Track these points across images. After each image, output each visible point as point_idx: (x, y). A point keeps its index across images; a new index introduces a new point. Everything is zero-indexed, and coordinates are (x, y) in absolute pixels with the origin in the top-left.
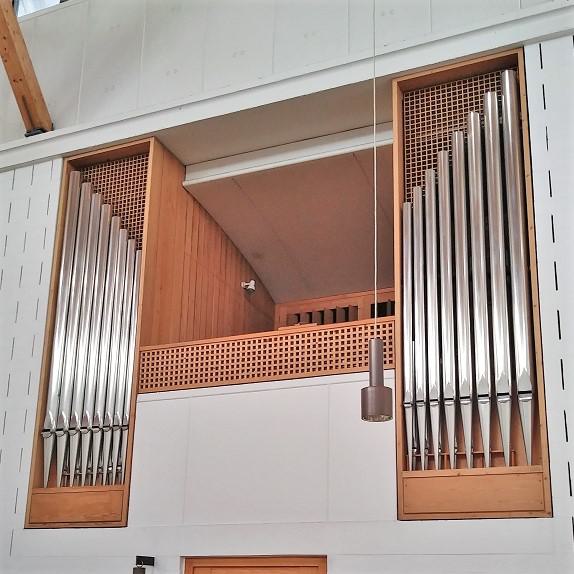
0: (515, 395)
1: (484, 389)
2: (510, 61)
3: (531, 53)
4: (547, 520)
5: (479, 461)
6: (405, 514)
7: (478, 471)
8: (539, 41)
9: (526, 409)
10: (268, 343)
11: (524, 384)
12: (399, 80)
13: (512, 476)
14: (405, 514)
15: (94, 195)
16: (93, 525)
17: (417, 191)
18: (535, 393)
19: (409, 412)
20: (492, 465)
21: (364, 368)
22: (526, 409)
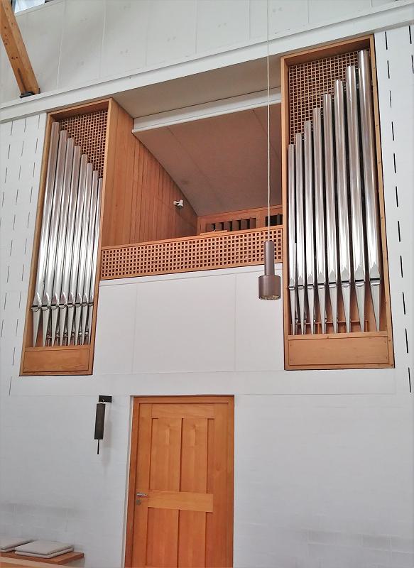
0: (368, 281)
2: (364, 44)
6: (290, 365)
7: (342, 335)
8: (385, 29)
10: (192, 245)
11: (375, 274)
14: (290, 365)
17: (298, 136)
18: (382, 280)
19: (293, 293)
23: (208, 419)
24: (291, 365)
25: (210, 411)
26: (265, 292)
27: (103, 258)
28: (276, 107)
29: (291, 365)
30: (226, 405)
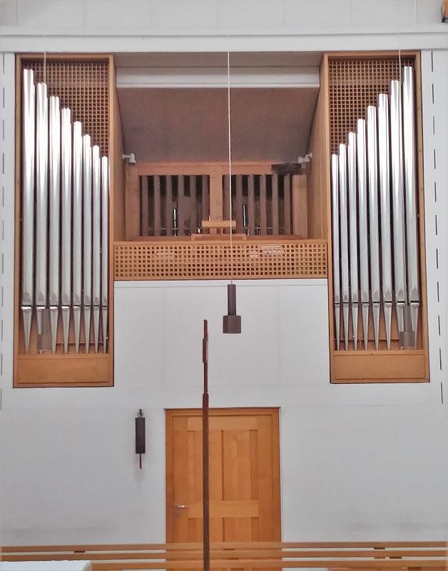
0: (371, 303)
1: (96, 302)
2: (410, 59)
3: (425, 58)
4: (426, 384)
5: (92, 347)
6: (335, 379)
7: (384, 352)
8: (432, 50)
9: (105, 313)
10: (227, 250)
11: (105, 304)
12: (330, 55)
13: (406, 356)
14: (335, 379)
15: (40, 85)
16: (30, 385)
17: (342, 147)
18: (420, 302)
19: (338, 310)
20: (391, 349)
21: (322, 275)
22: (105, 313)
23: (251, 430)
24: (336, 378)
25: (251, 422)
26: (88, 362)
27: (116, 255)
28: (316, 93)
29: (336, 378)
30: (269, 417)
